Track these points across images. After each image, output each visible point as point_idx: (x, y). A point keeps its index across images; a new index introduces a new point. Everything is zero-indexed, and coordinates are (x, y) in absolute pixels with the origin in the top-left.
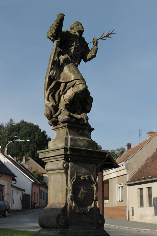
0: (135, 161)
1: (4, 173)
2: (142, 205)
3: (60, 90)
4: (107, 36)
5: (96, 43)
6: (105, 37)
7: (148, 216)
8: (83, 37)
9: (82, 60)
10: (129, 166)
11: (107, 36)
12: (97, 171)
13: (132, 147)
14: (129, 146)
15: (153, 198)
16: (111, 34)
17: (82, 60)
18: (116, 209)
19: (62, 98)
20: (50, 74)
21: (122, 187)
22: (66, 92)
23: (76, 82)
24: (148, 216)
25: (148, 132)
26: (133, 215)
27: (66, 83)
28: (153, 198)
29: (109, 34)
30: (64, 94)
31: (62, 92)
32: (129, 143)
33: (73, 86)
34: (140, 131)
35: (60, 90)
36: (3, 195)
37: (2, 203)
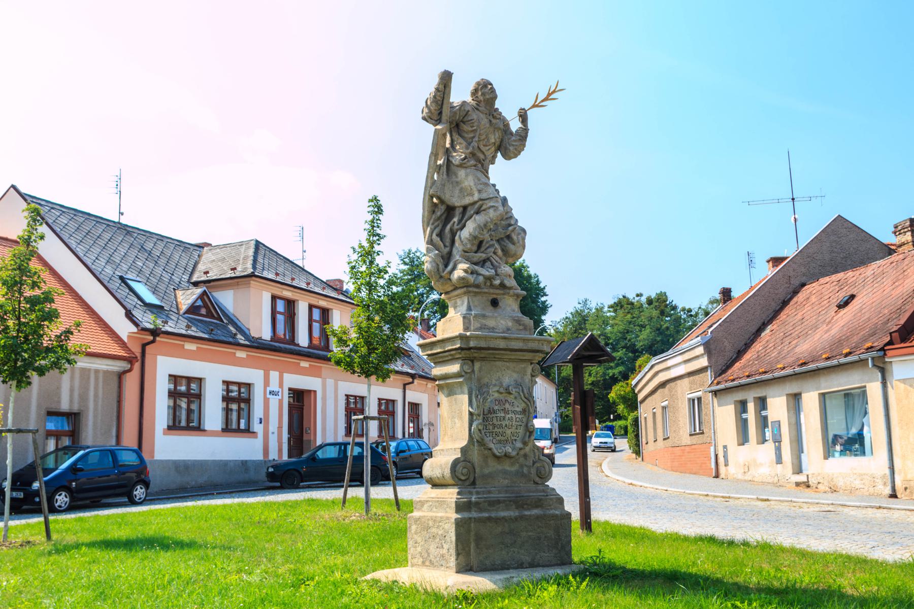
0: (730, 334)
1: (417, 376)
2: (743, 439)
3: (454, 222)
4: (546, 99)
5: (523, 116)
6: (542, 101)
7: (761, 464)
8: (497, 109)
9: (499, 154)
10: (712, 347)
11: (546, 99)
12: (532, 376)
13: (735, 294)
14: (726, 294)
15: (772, 422)
16: (554, 92)
17: (499, 154)
18: (689, 452)
19: (457, 238)
20: (431, 193)
21: (699, 399)
22: (464, 226)
23: (481, 206)
24: (761, 464)
25: (768, 258)
26: (726, 465)
27: (465, 208)
28: (772, 422)
29: (549, 94)
30: (462, 229)
31: (457, 225)
32: (726, 286)
33: (477, 212)
34: (751, 255)
35: (454, 222)
36: (420, 427)
37: (414, 446)
